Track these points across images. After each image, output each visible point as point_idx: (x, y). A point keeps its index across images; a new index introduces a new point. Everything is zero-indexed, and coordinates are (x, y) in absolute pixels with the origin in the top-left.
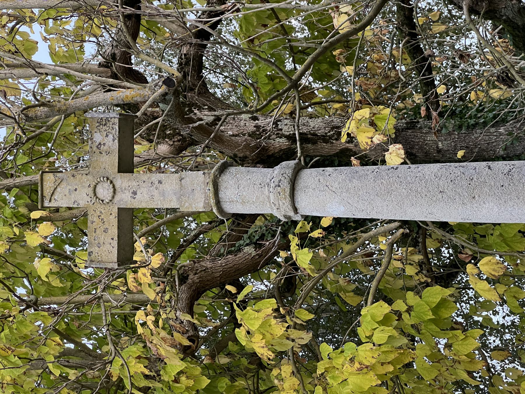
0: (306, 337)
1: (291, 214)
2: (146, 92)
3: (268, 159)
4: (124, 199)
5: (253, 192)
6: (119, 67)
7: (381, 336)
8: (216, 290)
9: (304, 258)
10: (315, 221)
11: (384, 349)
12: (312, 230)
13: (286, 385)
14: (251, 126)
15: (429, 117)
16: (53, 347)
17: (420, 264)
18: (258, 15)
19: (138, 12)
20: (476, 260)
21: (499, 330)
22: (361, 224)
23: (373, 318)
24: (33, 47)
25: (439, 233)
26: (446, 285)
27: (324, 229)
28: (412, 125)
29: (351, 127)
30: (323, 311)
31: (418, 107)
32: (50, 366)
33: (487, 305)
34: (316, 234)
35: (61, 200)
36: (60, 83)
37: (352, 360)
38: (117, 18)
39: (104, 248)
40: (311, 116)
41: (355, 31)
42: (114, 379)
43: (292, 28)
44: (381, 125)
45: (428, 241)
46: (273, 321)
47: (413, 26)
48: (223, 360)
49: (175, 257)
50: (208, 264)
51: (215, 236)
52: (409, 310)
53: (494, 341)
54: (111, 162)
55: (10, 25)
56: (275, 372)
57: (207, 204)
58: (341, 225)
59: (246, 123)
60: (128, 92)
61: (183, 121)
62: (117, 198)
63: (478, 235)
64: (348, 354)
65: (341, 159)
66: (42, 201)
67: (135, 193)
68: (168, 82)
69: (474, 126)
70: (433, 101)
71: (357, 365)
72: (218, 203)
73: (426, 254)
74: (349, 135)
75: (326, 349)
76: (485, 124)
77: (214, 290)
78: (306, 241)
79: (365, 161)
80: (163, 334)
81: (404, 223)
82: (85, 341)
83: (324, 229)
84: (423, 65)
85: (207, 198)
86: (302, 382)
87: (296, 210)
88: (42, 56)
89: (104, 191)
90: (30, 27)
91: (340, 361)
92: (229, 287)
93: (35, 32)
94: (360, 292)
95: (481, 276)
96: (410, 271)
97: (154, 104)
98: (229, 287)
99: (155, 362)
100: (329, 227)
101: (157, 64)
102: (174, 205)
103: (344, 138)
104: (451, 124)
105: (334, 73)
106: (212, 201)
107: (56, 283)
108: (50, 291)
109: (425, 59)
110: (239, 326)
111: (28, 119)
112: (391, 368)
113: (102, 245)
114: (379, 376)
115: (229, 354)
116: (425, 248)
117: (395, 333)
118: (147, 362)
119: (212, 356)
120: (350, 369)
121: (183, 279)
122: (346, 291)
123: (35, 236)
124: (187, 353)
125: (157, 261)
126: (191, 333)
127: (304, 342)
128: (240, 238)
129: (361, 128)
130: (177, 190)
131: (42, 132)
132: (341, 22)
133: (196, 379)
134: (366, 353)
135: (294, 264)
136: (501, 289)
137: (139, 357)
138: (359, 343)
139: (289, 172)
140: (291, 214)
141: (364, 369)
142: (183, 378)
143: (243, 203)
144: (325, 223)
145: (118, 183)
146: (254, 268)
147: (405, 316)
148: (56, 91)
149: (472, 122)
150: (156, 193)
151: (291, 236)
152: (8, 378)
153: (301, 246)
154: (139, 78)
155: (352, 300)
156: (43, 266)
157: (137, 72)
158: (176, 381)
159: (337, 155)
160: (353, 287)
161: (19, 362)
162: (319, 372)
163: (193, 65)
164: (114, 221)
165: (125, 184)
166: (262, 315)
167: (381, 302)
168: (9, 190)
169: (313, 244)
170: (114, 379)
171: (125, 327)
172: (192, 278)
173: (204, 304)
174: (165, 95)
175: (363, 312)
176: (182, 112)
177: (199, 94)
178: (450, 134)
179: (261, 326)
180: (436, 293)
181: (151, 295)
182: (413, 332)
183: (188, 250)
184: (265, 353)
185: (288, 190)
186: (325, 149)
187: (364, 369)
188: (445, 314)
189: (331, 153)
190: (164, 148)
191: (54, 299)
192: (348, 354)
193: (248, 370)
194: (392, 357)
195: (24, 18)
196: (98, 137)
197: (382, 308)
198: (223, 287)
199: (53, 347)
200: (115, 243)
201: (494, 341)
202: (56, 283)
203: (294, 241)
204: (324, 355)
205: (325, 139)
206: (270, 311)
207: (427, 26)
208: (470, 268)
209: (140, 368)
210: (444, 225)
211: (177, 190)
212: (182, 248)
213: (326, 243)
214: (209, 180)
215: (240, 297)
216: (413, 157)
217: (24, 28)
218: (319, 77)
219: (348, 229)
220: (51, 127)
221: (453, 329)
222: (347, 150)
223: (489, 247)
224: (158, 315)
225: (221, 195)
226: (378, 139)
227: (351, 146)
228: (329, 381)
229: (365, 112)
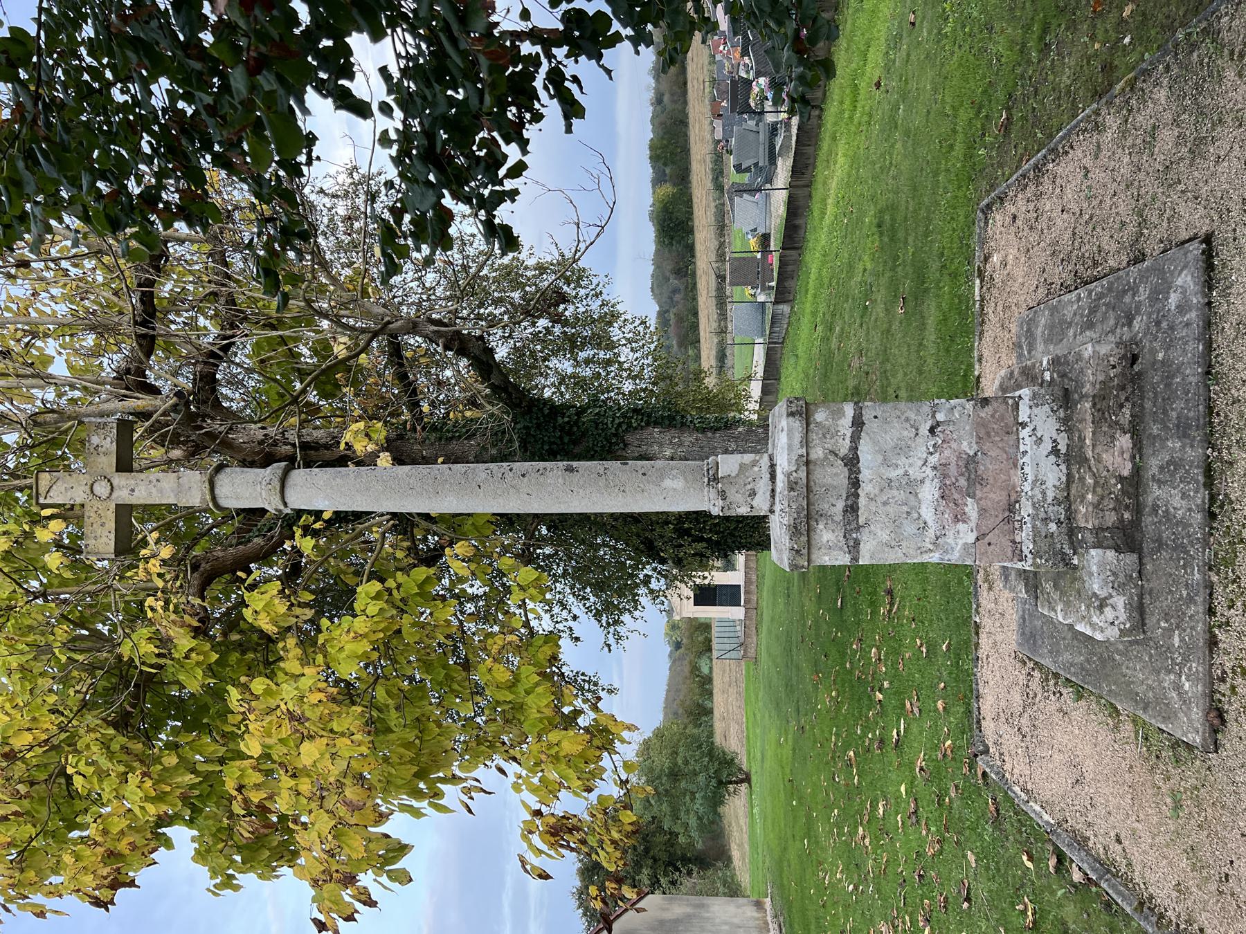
0: (309, 613)
1: (282, 507)
2: (158, 402)
3: (266, 460)
4: (123, 496)
5: (246, 489)
6: (134, 380)
7: (373, 609)
8: (227, 576)
9: (307, 545)
10: (318, 514)
11: (375, 619)
12: (315, 522)
13: (290, 655)
14: (260, 435)
15: (414, 429)
16: (62, 632)
17: (409, 549)
18: (269, 339)
19: (152, 332)
20: (451, 544)
21: (474, 598)
22: (358, 516)
23: (367, 594)
24: (49, 360)
25: (424, 524)
26: (429, 566)
27: (325, 521)
28: (401, 437)
29: (348, 437)
30: (328, 591)
31: (406, 421)
32: (56, 651)
33: (462, 580)
34: (317, 526)
35: (57, 497)
36: (77, 394)
37: (349, 631)
38: (129, 337)
39: (104, 539)
40: (316, 428)
41: (349, 358)
42: (125, 659)
43: (301, 355)
44: (375, 436)
45: (415, 530)
46: (277, 601)
47: (400, 357)
48: (235, 637)
49: (189, 549)
50: (220, 554)
51: (226, 530)
52: (399, 586)
53: (470, 608)
54: (108, 462)
55: (26, 340)
56: (281, 645)
57: (203, 500)
58: (341, 518)
59: (256, 431)
60: (139, 402)
61: (197, 427)
62: (115, 495)
63: (455, 524)
64: (345, 626)
65: (342, 461)
66: (37, 499)
67: (133, 490)
68: (179, 394)
69: (452, 438)
70: (418, 417)
71: (352, 634)
72: (214, 499)
73: (413, 542)
74: (346, 444)
75: (325, 622)
76: (460, 437)
77: (226, 576)
78: (307, 531)
79: (359, 464)
80: (173, 616)
81: (394, 515)
82: (100, 626)
83: (325, 521)
84: (411, 390)
85: (203, 494)
86: (305, 651)
87: (285, 505)
88: (59, 368)
89: (102, 489)
90: (45, 343)
91: (338, 632)
92: (239, 573)
93: (51, 347)
94: (358, 574)
95: (456, 557)
96: (400, 554)
97: (164, 414)
98: (239, 573)
99: (164, 642)
100: (330, 519)
101: (169, 377)
102: (172, 501)
103: (342, 446)
104: (433, 436)
105: (337, 393)
106: (208, 497)
107: (68, 574)
108: (64, 583)
109: (410, 384)
110: (247, 606)
111: (36, 424)
112: (382, 635)
113: (101, 540)
114: (371, 643)
115: (241, 632)
116: (413, 536)
117: (385, 606)
118: (158, 643)
119: (225, 634)
120: (347, 639)
121: (195, 567)
122: (345, 573)
123: (46, 532)
124: (197, 632)
125: (166, 552)
126: (202, 615)
127: (306, 618)
128: (250, 531)
129: (355, 437)
130: (182, 488)
131: (53, 439)
132: (339, 351)
133: (205, 654)
134: (360, 624)
135: (299, 551)
136: (473, 566)
137: (150, 638)
138: (355, 616)
139: (280, 472)
140: (282, 507)
141: (358, 637)
142: (193, 655)
143: (237, 498)
144: (326, 516)
145: (115, 482)
146: (264, 557)
147: (395, 592)
148: (73, 401)
149: (450, 435)
150: (154, 490)
151: (295, 528)
152: (15, 664)
153: (304, 536)
154: (154, 391)
155: (350, 580)
156: (54, 560)
157: (154, 386)
158: (187, 657)
159: (336, 460)
160: (353, 569)
161: (28, 649)
162: (320, 642)
163: (207, 382)
164: (111, 515)
165: (123, 483)
166: (267, 597)
167: (374, 582)
168: (21, 490)
169: (316, 534)
170: (125, 659)
171: (136, 615)
172: (204, 566)
173: (217, 587)
174: (175, 405)
175: (359, 589)
176: (191, 420)
177: (213, 406)
178: (432, 444)
179: (266, 605)
180: (422, 572)
181: (160, 583)
182: (401, 605)
183: (202, 541)
184: (270, 629)
185: (278, 488)
186: (327, 455)
187: (358, 637)
188: (428, 588)
189: (324, 455)
190: (177, 453)
191: (67, 589)
192: (345, 626)
193: (258, 645)
194: (382, 625)
195: (38, 333)
196: (95, 440)
197: (376, 586)
198: (234, 573)
199: (62, 632)
200: (112, 536)
201: (470, 608)
202: (68, 574)
203: (298, 532)
204: (324, 628)
205: (327, 447)
206: (275, 592)
207: (414, 359)
208: (447, 550)
209: (151, 648)
210: (427, 517)
211: (182, 488)
212: (195, 541)
213: (328, 533)
214: (206, 478)
215: (249, 581)
216: (399, 460)
217: (39, 343)
218: (324, 395)
219: (347, 522)
220: (66, 432)
221: (435, 600)
222: (346, 456)
223: (464, 534)
224: (167, 602)
225: (217, 492)
226: (371, 447)
227: (349, 453)
228: (329, 650)
229: (361, 425)
